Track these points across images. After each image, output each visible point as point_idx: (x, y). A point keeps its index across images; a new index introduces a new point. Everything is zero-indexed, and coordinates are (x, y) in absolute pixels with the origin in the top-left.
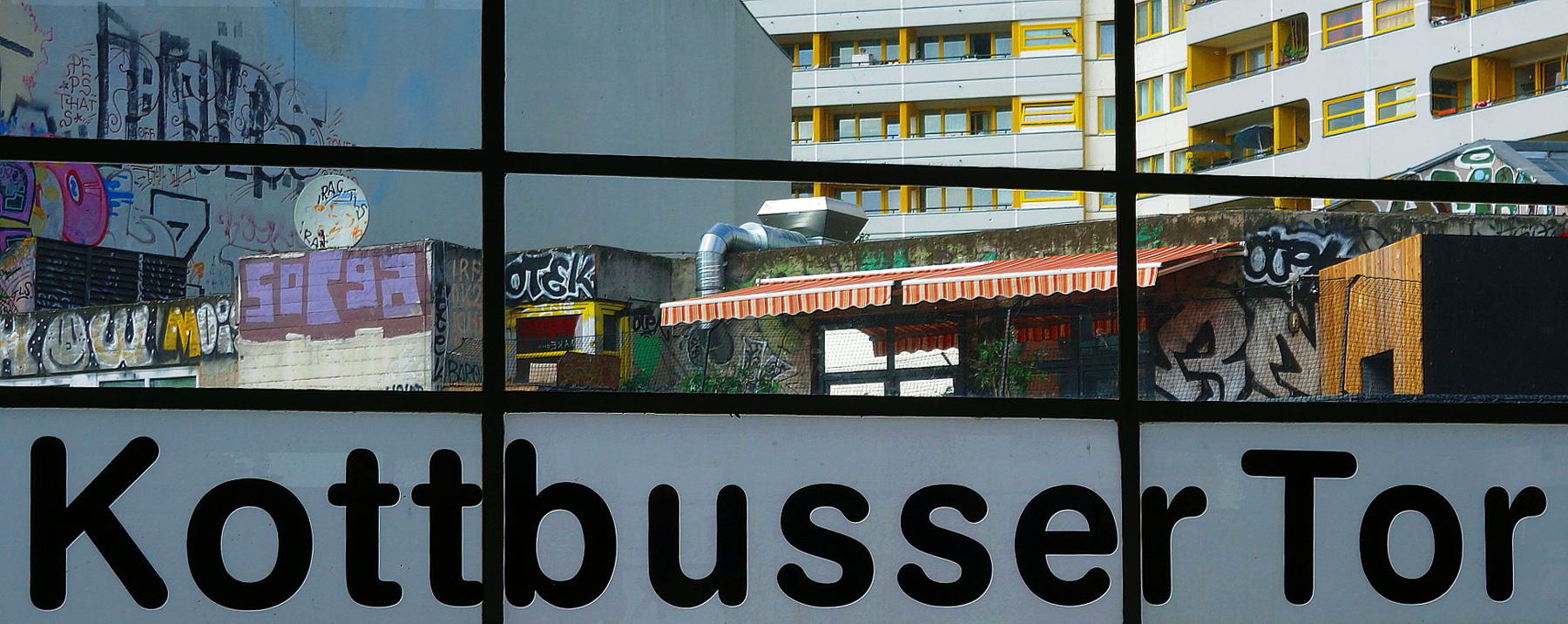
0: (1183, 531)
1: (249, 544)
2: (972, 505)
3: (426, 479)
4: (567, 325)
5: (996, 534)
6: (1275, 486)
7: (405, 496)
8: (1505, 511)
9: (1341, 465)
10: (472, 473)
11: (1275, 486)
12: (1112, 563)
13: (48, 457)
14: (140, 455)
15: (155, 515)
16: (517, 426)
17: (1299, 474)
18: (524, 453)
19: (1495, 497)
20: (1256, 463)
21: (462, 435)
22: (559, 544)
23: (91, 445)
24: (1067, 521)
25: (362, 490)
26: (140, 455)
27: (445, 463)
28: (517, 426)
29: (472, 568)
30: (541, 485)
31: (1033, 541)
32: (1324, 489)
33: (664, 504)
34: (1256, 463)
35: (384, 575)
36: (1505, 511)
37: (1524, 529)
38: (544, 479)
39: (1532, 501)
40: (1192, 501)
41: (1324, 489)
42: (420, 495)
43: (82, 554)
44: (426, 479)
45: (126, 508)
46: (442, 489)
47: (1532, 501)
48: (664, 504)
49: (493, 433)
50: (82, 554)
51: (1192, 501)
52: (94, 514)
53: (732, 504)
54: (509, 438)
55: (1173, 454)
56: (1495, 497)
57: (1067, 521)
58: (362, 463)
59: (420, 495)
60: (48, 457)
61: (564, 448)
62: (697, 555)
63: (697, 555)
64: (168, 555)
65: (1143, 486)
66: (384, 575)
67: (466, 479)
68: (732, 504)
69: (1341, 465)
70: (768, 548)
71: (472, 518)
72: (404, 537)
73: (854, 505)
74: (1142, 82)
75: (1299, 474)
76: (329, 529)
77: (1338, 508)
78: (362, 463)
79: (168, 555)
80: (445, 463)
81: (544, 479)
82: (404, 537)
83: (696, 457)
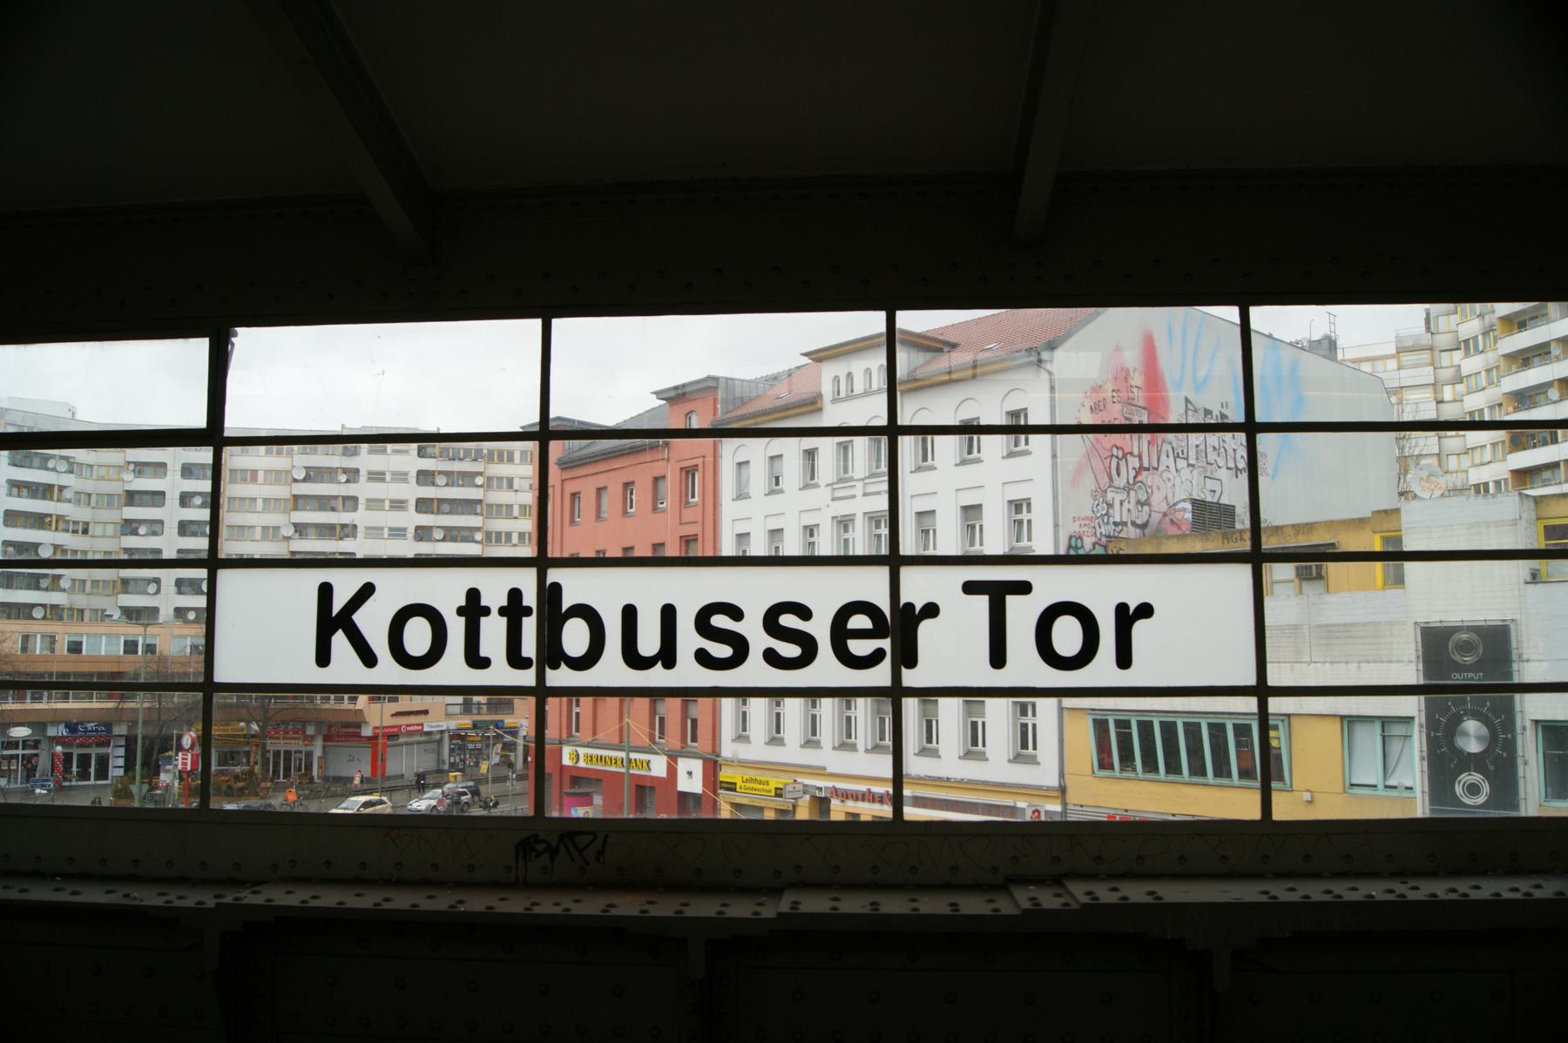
0: (926, 629)
1: (418, 637)
2: (804, 612)
3: (483, 620)
4: (352, 779)
5: (820, 628)
6: (982, 602)
7: (495, 611)
8: (1126, 618)
9: (1024, 588)
10: (530, 599)
11: (982, 602)
12: (885, 644)
13: (326, 591)
14: (367, 591)
15: (373, 621)
16: (554, 575)
17: (998, 594)
18: (556, 589)
19: (1121, 609)
20: (970, 588)
21: (526, 580)
22: (575, 637)
23: (345, 584)
24: (860, 622)
25: (473, 609)
26: (367, 591)
27: (515, 595)
28: (554, 575)
29: (529, 648)
30: (566, 605)
31: (840, 633)
32: (1012, 601)
33: (630, 614)
34: (970, 588)
35: (483, 653)
36: (1126, 618)
37: (1140, 629)
38: (567, 603)
39: (1145, 611)
40: (931, 610)
41: (1012, 601)
42: (502, 611)
43: (340, 640)
44: (483, 620)
45: (358, 617)
46: (514, 609)
47: (1145, 611)
48: (630, 614)
49: (541, 578)
50: (340, 640)
51: (931, 610)
52: (345, 622)
53: (669, 613)
54: (549, 582)
55: (918, 586)
56: (1121, 609)
57: (860, 622)
58: (473, 595)
59: (502, 611)
60: (326, 591)
61: (576, 586)
62: (649, 643)
63: (649, 643)
64: (379, 642)
65: (902, 602)
66: (483, 653)
67: (525, 603)
68: (669, 613)
69: (1024, 588)
70: (688, 639)
71: (529, 626)
72: (493, 632)
73: (736, 613)
74: (879, 391)
75: (998, 594)
76: (456, 628)
77: (1022, 614)
78: (473, 595)
79: (379, 642)
80: (515, 595)
81: (567, 603)
82: (493, 632)
83: (649, 590)
